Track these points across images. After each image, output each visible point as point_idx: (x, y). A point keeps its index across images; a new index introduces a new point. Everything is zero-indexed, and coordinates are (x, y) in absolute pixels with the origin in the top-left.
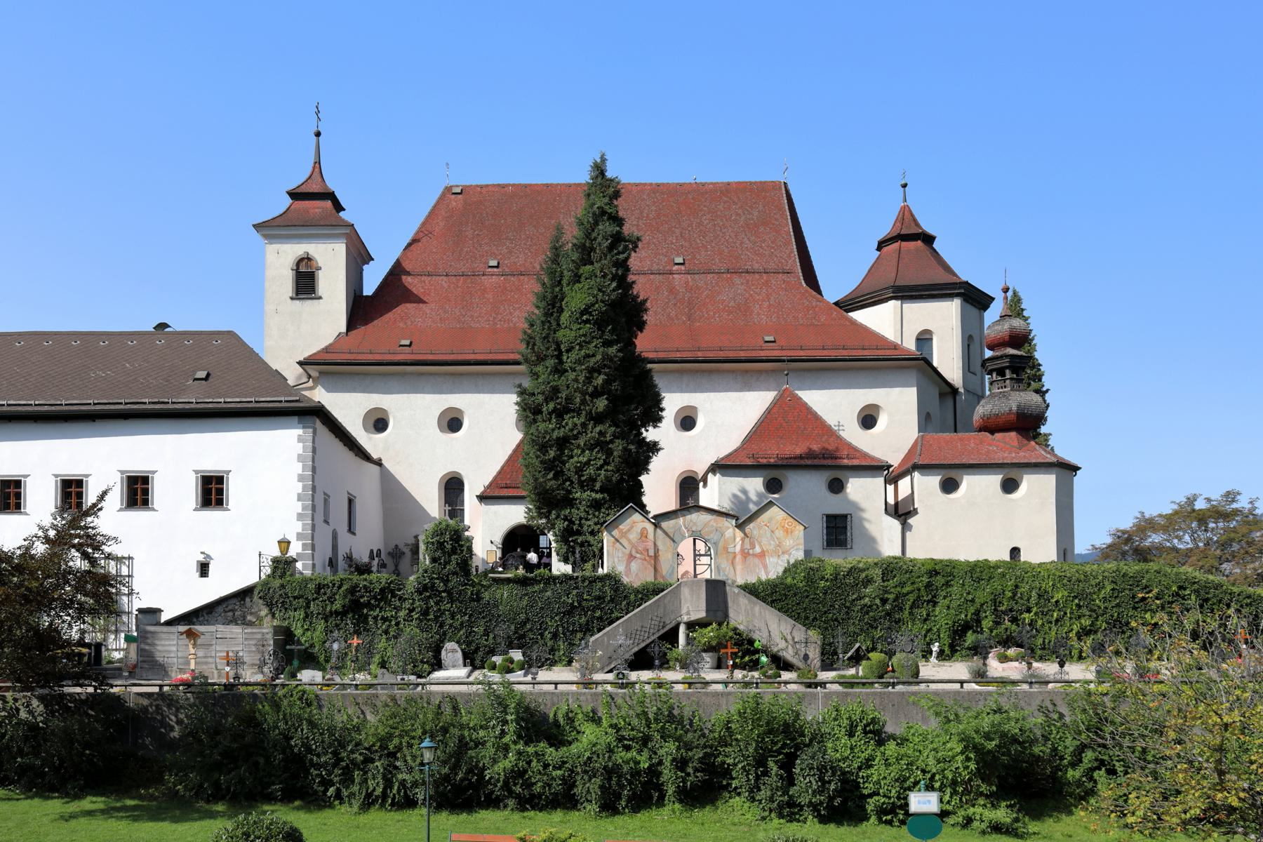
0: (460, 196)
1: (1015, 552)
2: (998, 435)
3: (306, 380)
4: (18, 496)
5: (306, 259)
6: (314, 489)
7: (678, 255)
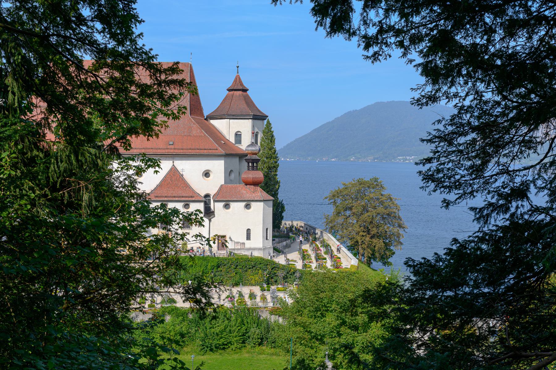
2: (248, 186)
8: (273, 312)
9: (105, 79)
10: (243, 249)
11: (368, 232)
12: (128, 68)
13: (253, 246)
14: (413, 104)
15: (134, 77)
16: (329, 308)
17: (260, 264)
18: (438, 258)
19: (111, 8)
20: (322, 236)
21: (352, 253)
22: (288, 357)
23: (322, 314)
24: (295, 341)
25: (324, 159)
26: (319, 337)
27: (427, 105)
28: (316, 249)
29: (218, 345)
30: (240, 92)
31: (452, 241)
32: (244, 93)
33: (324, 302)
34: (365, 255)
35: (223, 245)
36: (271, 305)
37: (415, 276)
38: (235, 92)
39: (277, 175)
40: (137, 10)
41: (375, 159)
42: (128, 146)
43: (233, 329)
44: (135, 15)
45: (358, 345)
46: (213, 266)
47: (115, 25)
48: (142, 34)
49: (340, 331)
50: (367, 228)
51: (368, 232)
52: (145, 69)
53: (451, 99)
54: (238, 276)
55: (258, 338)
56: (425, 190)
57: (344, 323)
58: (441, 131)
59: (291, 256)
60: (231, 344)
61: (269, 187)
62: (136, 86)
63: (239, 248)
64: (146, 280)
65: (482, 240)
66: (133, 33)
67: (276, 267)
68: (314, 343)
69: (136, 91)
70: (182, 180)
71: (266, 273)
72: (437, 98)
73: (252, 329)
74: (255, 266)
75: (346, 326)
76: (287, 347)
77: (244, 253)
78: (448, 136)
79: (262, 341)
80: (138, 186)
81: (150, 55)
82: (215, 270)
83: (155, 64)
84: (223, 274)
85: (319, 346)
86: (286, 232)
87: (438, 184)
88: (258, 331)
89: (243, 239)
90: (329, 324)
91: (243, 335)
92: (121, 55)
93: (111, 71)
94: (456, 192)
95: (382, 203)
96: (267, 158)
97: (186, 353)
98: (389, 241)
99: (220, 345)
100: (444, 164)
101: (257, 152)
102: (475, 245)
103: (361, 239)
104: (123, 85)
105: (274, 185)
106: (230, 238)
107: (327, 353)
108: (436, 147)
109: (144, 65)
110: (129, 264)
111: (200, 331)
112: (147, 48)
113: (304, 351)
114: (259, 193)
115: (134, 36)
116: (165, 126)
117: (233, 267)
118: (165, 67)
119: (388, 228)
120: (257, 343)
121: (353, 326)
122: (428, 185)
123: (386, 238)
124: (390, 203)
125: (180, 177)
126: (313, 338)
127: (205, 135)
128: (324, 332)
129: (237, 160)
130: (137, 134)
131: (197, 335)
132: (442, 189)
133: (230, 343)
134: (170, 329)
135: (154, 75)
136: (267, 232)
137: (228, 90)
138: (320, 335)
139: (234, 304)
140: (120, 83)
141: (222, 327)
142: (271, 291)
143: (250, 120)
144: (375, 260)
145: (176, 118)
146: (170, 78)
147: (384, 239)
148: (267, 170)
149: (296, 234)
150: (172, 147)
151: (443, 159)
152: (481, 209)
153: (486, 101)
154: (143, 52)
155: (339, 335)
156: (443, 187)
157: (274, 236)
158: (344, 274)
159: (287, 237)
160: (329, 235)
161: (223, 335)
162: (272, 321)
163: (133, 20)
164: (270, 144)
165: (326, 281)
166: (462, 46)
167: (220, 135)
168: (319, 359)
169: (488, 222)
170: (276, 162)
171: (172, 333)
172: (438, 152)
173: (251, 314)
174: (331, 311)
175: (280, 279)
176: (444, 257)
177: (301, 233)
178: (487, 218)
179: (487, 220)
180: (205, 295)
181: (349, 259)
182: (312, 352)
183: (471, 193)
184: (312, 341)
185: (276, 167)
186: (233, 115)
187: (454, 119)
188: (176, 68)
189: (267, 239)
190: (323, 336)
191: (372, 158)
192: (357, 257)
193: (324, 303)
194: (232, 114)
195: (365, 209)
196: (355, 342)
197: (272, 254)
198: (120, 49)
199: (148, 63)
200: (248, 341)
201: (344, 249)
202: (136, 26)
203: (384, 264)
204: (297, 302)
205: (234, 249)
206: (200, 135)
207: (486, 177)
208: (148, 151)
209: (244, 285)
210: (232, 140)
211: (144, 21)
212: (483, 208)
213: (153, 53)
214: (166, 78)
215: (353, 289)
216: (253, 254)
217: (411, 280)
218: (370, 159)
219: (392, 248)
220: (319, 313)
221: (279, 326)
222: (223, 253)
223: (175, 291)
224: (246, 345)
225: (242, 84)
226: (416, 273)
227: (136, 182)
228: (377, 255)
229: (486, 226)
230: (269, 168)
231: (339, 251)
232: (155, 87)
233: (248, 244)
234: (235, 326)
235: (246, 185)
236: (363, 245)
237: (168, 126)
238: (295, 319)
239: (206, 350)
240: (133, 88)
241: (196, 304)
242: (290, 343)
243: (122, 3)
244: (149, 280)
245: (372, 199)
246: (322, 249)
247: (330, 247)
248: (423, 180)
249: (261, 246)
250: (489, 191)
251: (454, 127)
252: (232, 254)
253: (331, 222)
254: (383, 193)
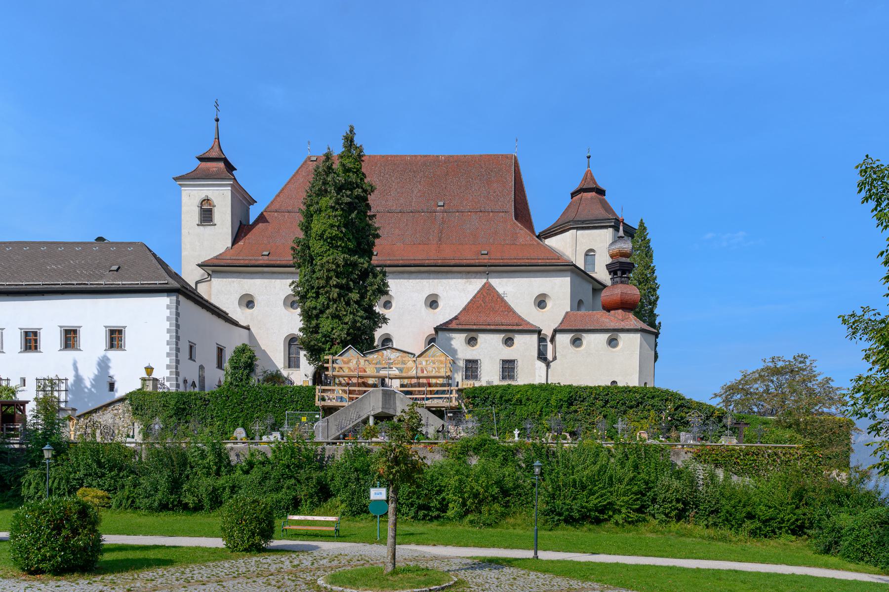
0: (315, 162)
1: (645, 384)
2: (612, 312)
3: (207, 277)
4: (36, 341)
5: (207, 200)
6: (178, 338)
7: (441, 201)
17: (653, 397)
30: (593, 194)
46: (561, 400)
55: (678, 501)
74: (641, 403)
84: (580, 417)
114: (631, 320)
117: (599, 403)
120: (674, 513)
150: (486, 257)
206: (531, 243)
235: (609, 311)
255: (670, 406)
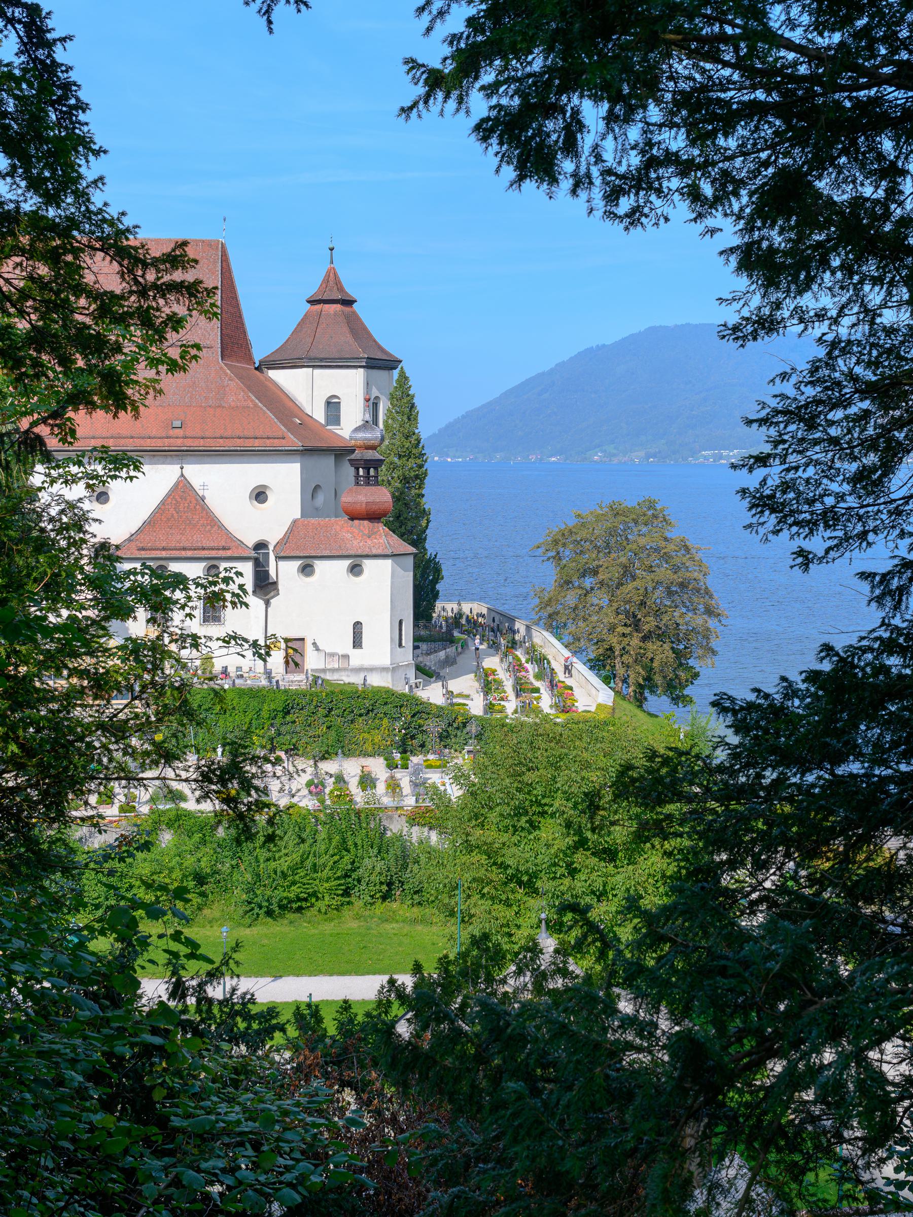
2: (356, 522)
8: (416, 818)
9: (16, 282)
10: (345, 669)
11: (636, 625)
12: (69, 258)
13: (367, 662)
14: (724, 337)
15: (82, 277)
16: (546, 808)
17: (386, 704)
18: (790, 691)
19: (30, 125)
20: (530, 637)
21: (599, 676)
22: (453, 927)
23: (530, 822)
24: (469, 888)
25: (533, 458)
26: (525, 878)
27: (755, 339)
28: (517, 668)
29: (285, 902)
30: (338, 307)
31: (821, 651)
32: (347, 309)
33: (535, 792)
34: (631, 681)
35: (293, 662)
36: (410, 801)
37: (737, 733)
38: (326, 306)
39: (423, 496)
40: (90, 127)
41: (648, 456)
42: (68, 433)
43: (322, 861)
44: (84, 137)
45: (615, 896)
46: (275, 710)
47: (39, 160)
48: (101, 178)
49: (572, 863)
50: (635, 616)
51: (636, 625)
52: (108, 258)
53: (810, 324)
54: (333, 733)
55: (381, 883)
56: (757, 532)
57: (582, 843)
58: (788, 398)
59: (455, 685)
60: (317, 899)
61: (406, 524)
62: (87, 297)
63: (336, 666)
64: (109, 751)
65: (889, 646)
66: (80, 177)
67: (422, 710)
68: (513, 892)
69: (88, 309)
70: (203, 509)
71: (398, 725)
72: (779, 323)
73: (366, 860)
74: (372, 710)
75: (588, 849)
76: (449, 904)
77: (347, 680)
78: (806, 409)
79: (390, 890)
80: (92, 528)
81: (121, 226)
82: (278, 721)
83: (131, 247)
84: (298, 729)
85: (525, 898)
86: (444, 629)
87: (785, 516)
88: (380, 866)
89: (345, 645)
90: (548, 846)
91: (346, 876)
92: (53, 227)
93: (31, 263)
94: (828, 533)
95: (667, 557)
96: (400, 457)
97: (210, 922)
98: (686, 648)
99: (290, 902)
100: (796, 468)
101: (376, 443)
102: (876, 658)
103: (620, 643)
104: (57, 294)
105: (417, 518)
106: (314, 644)
107: (543, 916)
108: (781, 435)
109: (108, 249)
110: (68, 713)
111: (242, 867)
112: (113, 211)
113: (490, 913)
114: (381, 536)
115: (84, 184)
116: (155, 389)
117: (322, 712)
118: (156, 252)
119: (682, 615)
120: (378, 895)
121: (605, 851)
122: (762, 520)
123: (679, 640)
124: (685, 559)
125: (198, 503)
126: (511, 880)
127: (256, 405)
128: (536, 865)
129: (330, 461)
130: (91, 406)
131: (236, 876)
132: (795, 529)
133: (314, 894)
134: (170, 865)
135: (130, 271)
136: (400, 630)
137: (308, 302)
138: (527, 872)
139: (322, 802)
140: (51, 290)
141: (296, 857)
142: (410, 769)
143: (361, 370)
144: (652, 692)
145: (174, 367)
146: (167, 278)
147: (672, 642)
148: (399, 486)
149: (468, 633)
150: (179, 432)
151: (793, 458)
152: (884, 576)
153: (891, 327)
154: (104, 220)
155: (573, 872)
156: (796, 523)
157: (417, 639)
158: (581, 725)
159: (448, 640)
160: (547, 634)
161: (297, 878)
162: (414, 840)
163: (81, 149)
164: (407, 426)
165: (540, 743)
166: (830, 202)
167: (291, 404)
168: (524, 932)
169: (903, 607)
170: (421, 466)
171: (177, 874)
172: (784, 442)
173: (364, 825)
174: (553, 815)
175: (432, 739)
176: (803, 686)
177: (480, 629)
178: (901, 595)
179: (900, 601)
180: (246, 785)
181: (594, 691)
182: (510, 913)
183: (863, 535)
184: (508, 889)
185: (420, 478)
186: (321, 360)
187: (817, 369)
188: (181, 256)
189: (400, 645)
190: (534, 876)
191: (642, 454)
192: (612, 685)
193: (536, 796)
194: (318, 356)
195: (627, 573)
196: (608, 888)
197: (413, 681)
198: (52, 213)
199: (115, 245)
200: (356, 889)
201: (580, 667)
202: (87, 162)
203: (676, 700)
204: (472, 794)
205: (324, 671)
207: (895, 500)
208: (122, 441)
209: (348, 754)
210: (319, 414)
211: (105, 152)
212: (889, 573)
213: (127, 222)
214: (158, 279)
215: (603, 762)
216: (368, 682)
217: (727, 744)
218: (637, 456)
219: (691, 662)
220: (524, 819)
221: (430, 852)
222: (296, 681)
223: (177, 775)
224: (353, 899)
225: (341, 289)
226: (739, 727)
227: (87, 520)
228: (658, 679)
229: (898, 615)
230: (405, 480)
231: (570, 672)
232: (133, 298)
233: (358, 658)
234: (326, 853)
235: (352, 519)
236: (625, 658)
237: (160, 392)
238: (468, 835)
239: (258, 915)
240: (83, 302)
241: (229, 806)
242: (456, 892)
243: (56, 110)
244: (117, 750)
245: (643, 548)
246: (529, 666)
247: (549, 663)
248: (750, 509)
249: (386, 661)
250: (902, 530)
251: (819, 389)
252: (320, 682)
253: (549, 603)
254: (668, 535)
255: (407, 712)
